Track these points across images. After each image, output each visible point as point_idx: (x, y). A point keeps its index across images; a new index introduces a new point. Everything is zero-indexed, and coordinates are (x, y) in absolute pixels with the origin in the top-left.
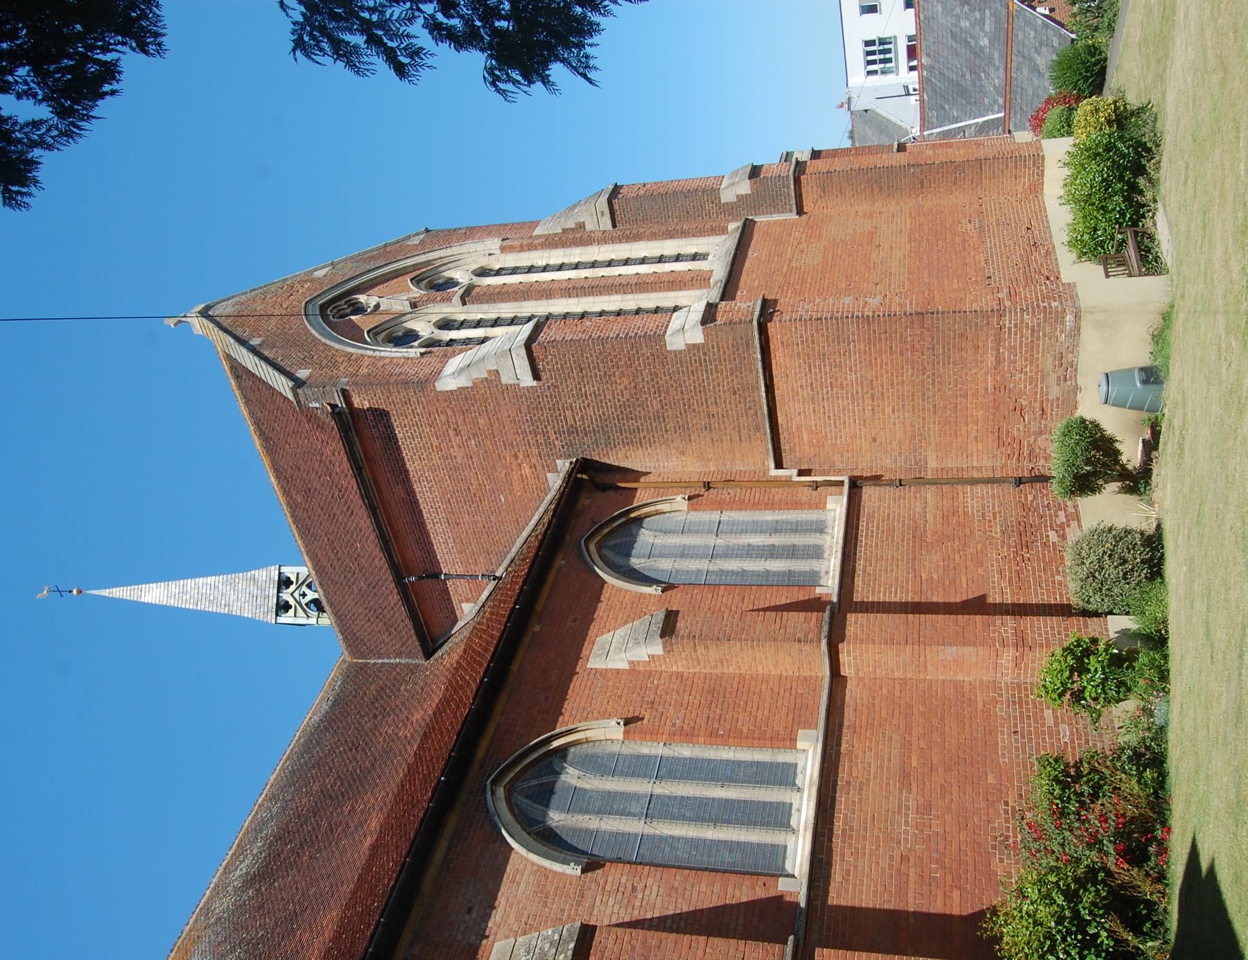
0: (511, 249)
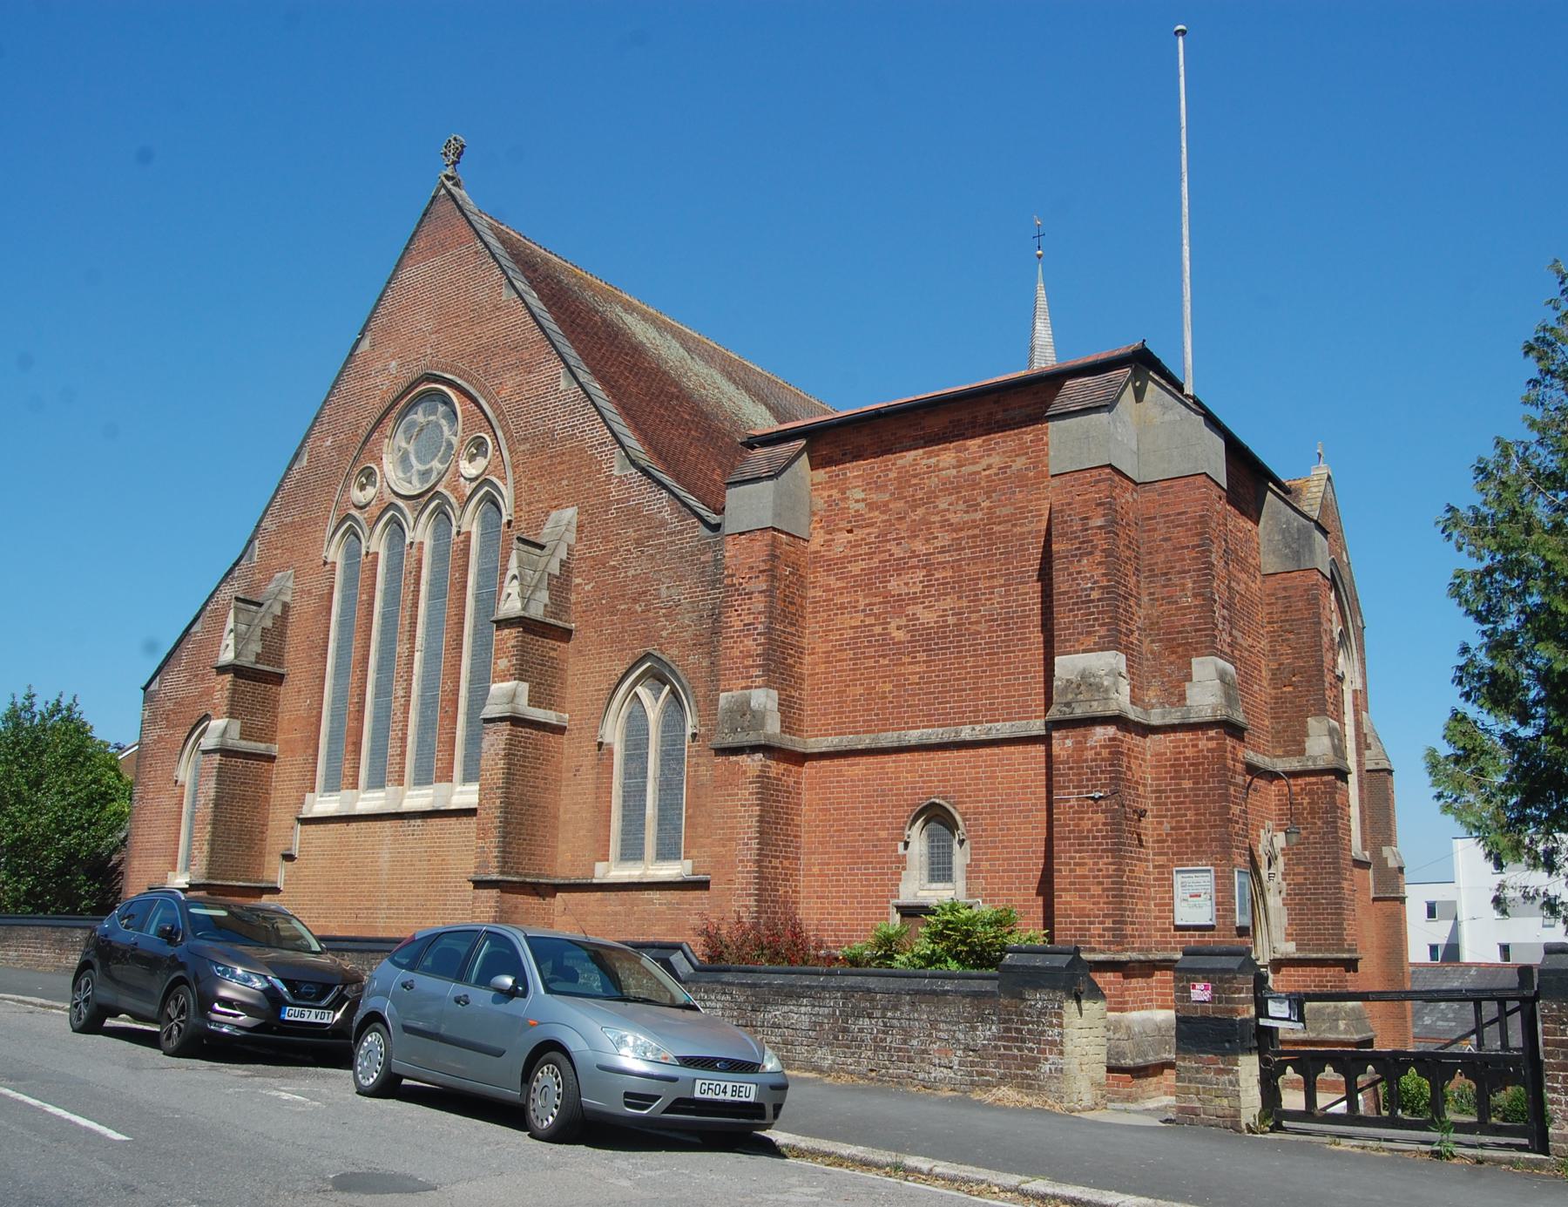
0: (1355, 698)
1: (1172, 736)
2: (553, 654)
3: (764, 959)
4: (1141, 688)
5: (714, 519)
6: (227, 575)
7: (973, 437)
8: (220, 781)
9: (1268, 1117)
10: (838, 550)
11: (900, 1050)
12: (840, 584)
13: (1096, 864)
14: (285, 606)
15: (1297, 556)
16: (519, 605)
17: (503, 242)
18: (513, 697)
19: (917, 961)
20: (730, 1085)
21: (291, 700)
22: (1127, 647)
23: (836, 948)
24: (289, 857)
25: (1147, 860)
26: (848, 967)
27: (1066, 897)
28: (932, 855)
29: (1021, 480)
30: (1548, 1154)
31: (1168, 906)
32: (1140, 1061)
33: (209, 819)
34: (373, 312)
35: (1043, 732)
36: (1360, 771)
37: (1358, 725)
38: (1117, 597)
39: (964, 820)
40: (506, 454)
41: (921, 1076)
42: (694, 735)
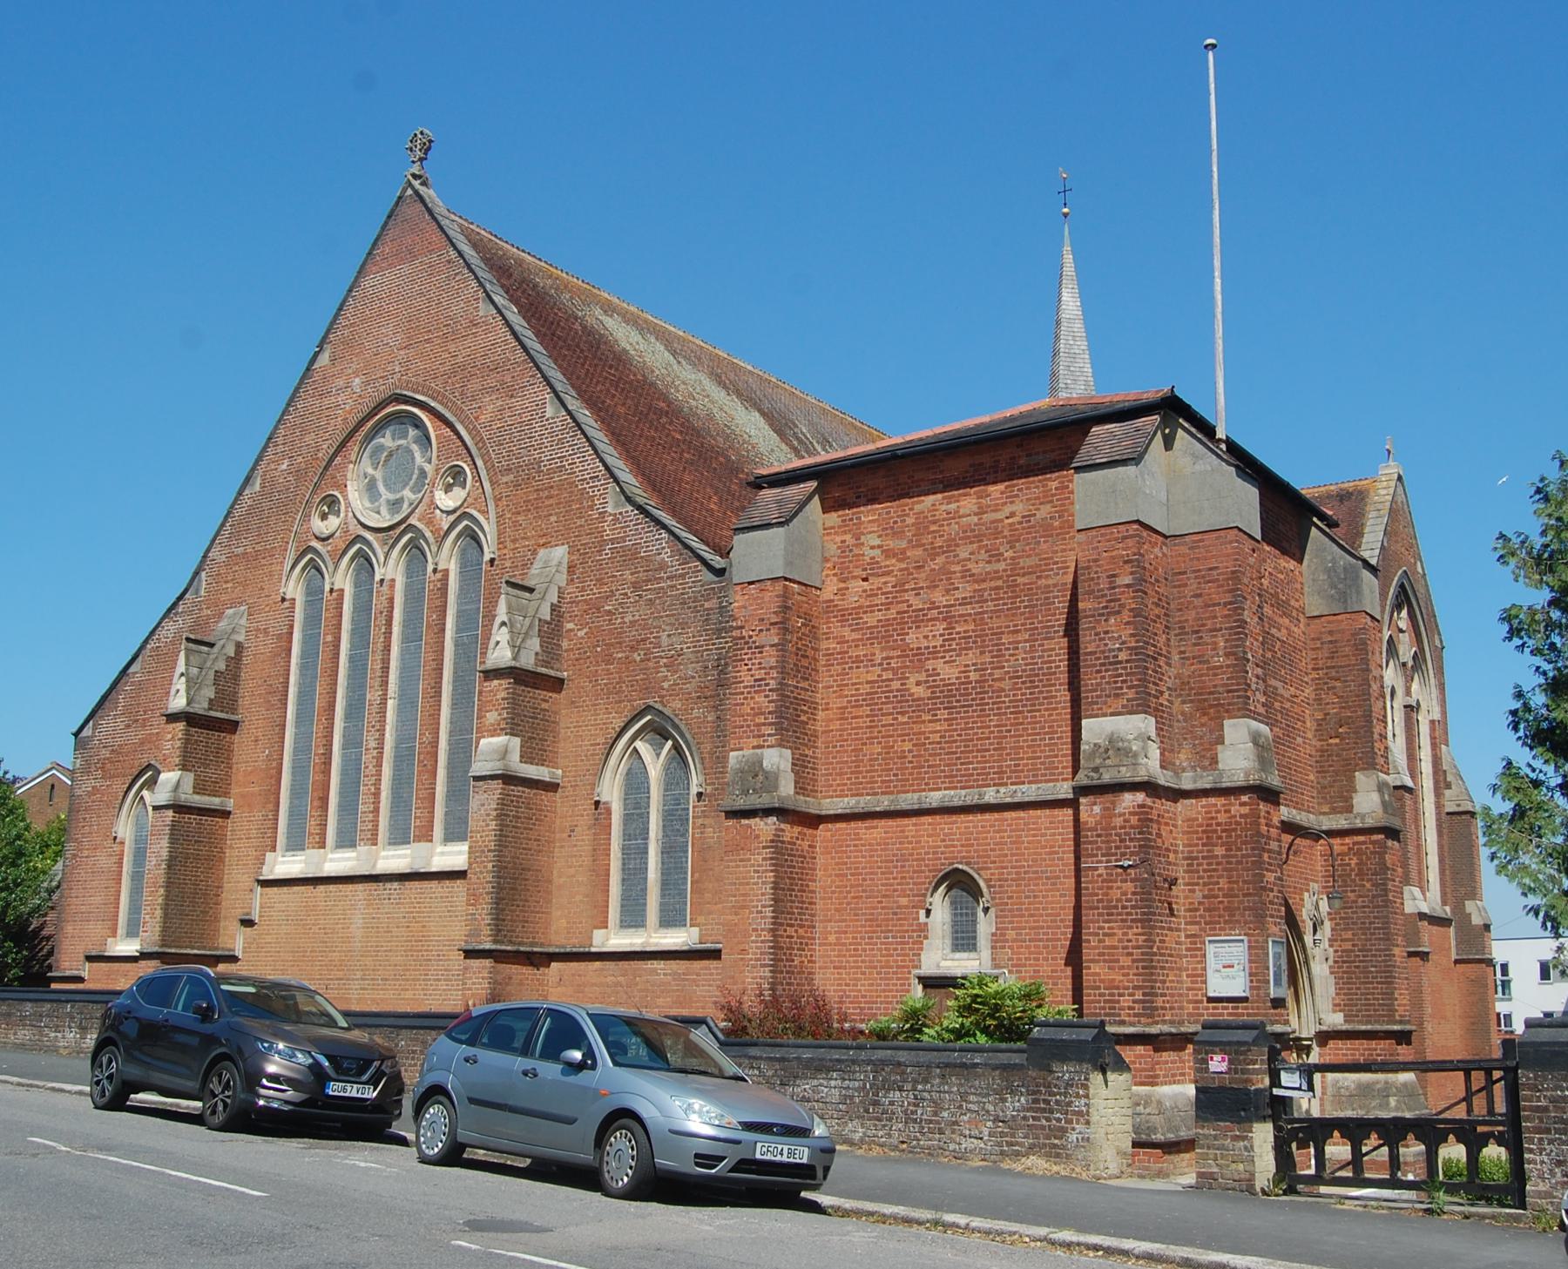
0: (1433, 729)
1: (1204, 801)
2: (545, 706)
3: (782, 1033)
4: (1172, 751)
5: (718, 562)
6: (170, 610)
7: (994, 483)
8: (173, 840)
9: (1281, 1181)
10: (852, 599)
11: (931, 1122)
12: (855, 636)
13: (1125, 934)
14: (239, 645)
15: (1343, 597)
16: (508, 654)
17: (475, 246)
18: (504, 753)
19: (946, 1036)
20: (786, 1148)
21: (246, 750)
22: (1156, 710)
23: (862, 1021)
24: (248, 923)
25: (1178, 930)
26: (874, 1041)
27: (1095, 968)
28: (955, 924)
29: (1046, 529)
30: (1523, 1206)
31: (1200, 977)
32: (1171, 1136)
33: (162, 880)
34: (333, 322)
35: (1071, 796)
36: (1438, 814)
37: (1436, 761)
38: (1145, 659)
39: (989, 887)
40: (487, 485)
41: (952, 1147)
42: (700, 795)
